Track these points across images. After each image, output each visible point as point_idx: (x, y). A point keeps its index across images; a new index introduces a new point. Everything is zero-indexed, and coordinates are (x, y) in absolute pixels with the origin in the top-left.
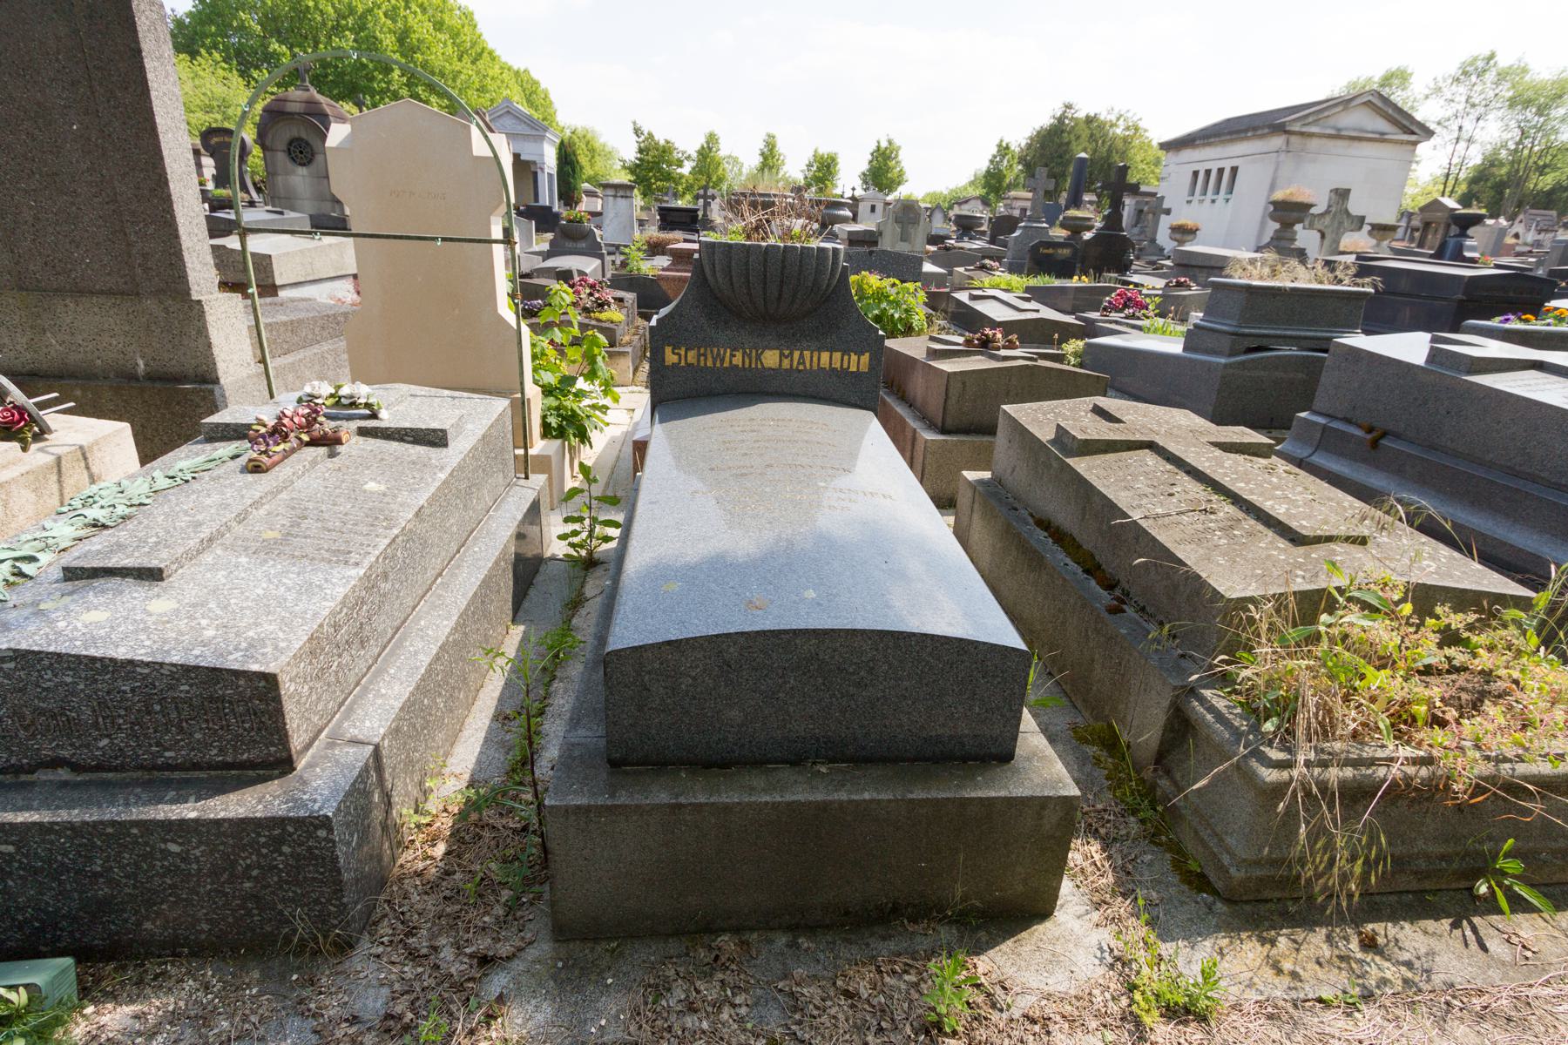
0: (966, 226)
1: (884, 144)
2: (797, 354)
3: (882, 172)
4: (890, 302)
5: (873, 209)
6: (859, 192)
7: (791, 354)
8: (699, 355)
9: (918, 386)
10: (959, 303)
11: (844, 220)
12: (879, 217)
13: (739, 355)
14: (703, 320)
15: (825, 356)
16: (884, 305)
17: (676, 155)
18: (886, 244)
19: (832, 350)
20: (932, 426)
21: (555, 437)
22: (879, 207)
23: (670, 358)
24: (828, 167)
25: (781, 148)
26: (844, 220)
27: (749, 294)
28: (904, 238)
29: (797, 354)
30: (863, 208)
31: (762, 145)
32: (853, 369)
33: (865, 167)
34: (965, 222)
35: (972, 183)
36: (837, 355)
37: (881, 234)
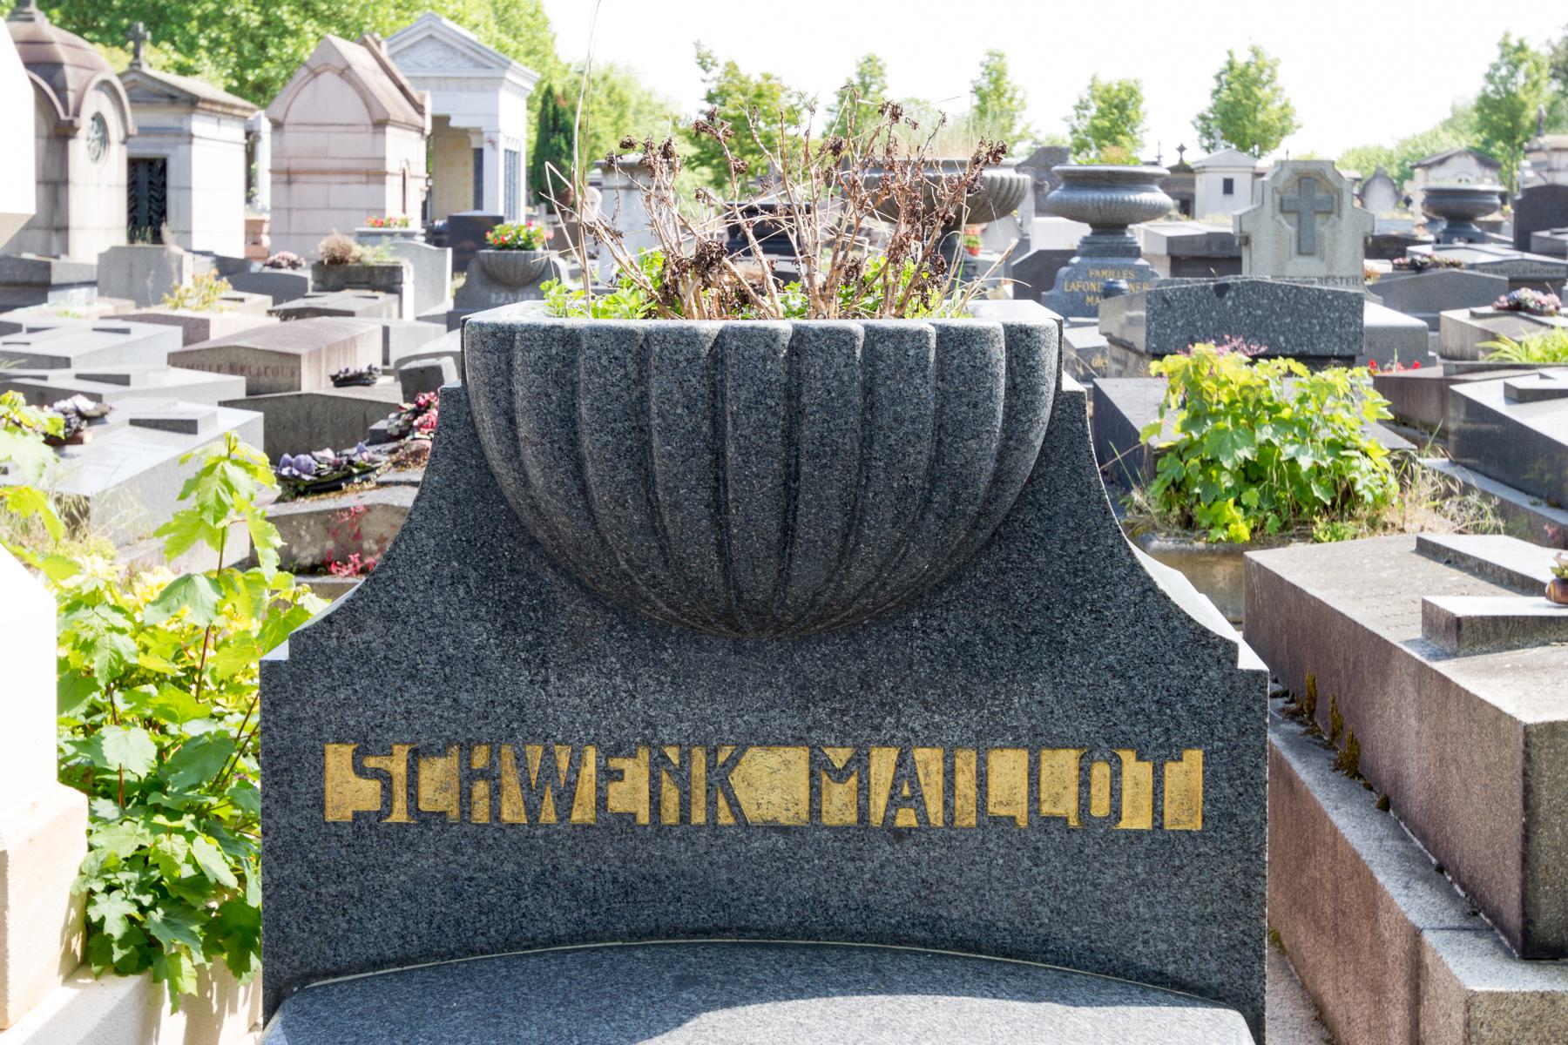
0: (1456, 213)
1: (1242, 58)
2: (883, 763)
3: (1238, 116)
4: (1283, 425)
5: (1228, 186)
6: (1194, 156)
7: (860, 761)
8: (469, 777)
9: (1401, 734)
10: (1477, 411)
11: (1155, 212)
12: (1242, 202)
13: (636, 771)
14: (479, 633)
15: (1008, 768)
16: (1265, 433)
17: (784, 103)
18: (1260, 267)
19: (1036, 742)
20: (1477, 912)
21: (121, 970)
22: (1242, 183)
23: (348, 791)
24: (1122, 107)
25: (1015, 77)
26: (1155, 212)
27: (655, 529)
28: (1306, 246)
29: (883, 763)
30: (1206, 188)
31: (976, 73)
32: (1136, 818)
33: (1205, 103)
34: (1450, 203)
35: (1448, 125)
36: (1061, 765)
37: (1246, 241)
